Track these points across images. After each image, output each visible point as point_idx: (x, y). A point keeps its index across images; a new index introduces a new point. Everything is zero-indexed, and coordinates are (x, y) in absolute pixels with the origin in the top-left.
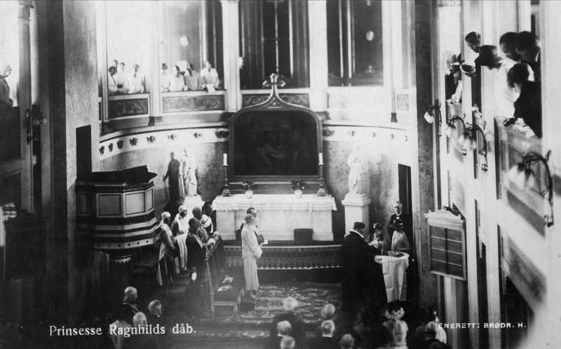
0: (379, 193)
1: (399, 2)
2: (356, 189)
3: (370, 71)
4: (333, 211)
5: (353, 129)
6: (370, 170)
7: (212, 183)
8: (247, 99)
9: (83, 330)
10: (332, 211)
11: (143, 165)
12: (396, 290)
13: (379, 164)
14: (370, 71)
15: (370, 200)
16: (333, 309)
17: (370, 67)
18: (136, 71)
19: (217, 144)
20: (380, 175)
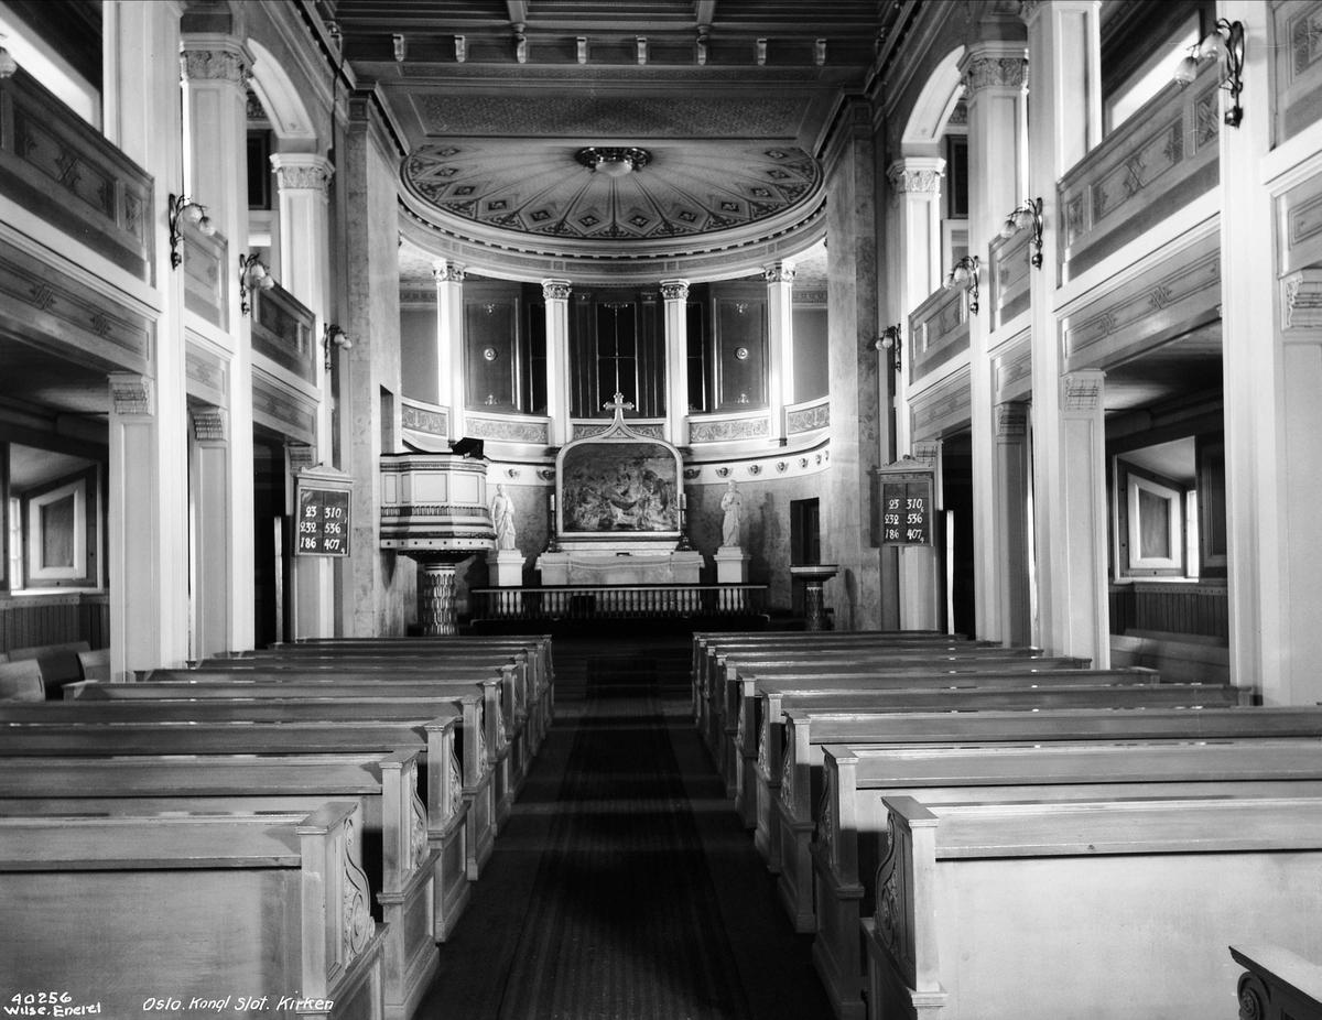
0: (762, 545)
1: (1263, 4)
2: (734, 539)
3: (743, 401)
4: (701, 569)
5: (758, 463)
6: (750, 517)
7: (532, 541)
8: (579, 432)
9: (45, 995)
10: (701, 569)
11: (788, 505)
12: (130, 208)
13: (761, 508)
14: (743, 401)
15: (1238, 677)
16: (274, 158)
17: (743, 395)
18: (251, 93)
19: (538, 487)
20: (763, 522)
